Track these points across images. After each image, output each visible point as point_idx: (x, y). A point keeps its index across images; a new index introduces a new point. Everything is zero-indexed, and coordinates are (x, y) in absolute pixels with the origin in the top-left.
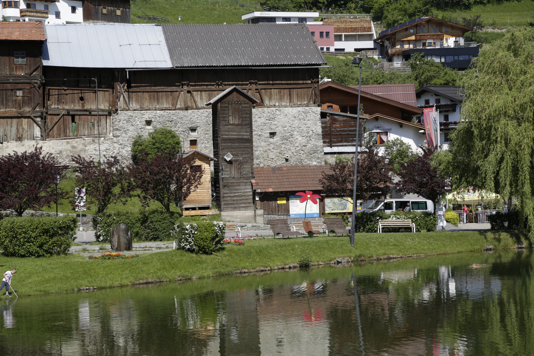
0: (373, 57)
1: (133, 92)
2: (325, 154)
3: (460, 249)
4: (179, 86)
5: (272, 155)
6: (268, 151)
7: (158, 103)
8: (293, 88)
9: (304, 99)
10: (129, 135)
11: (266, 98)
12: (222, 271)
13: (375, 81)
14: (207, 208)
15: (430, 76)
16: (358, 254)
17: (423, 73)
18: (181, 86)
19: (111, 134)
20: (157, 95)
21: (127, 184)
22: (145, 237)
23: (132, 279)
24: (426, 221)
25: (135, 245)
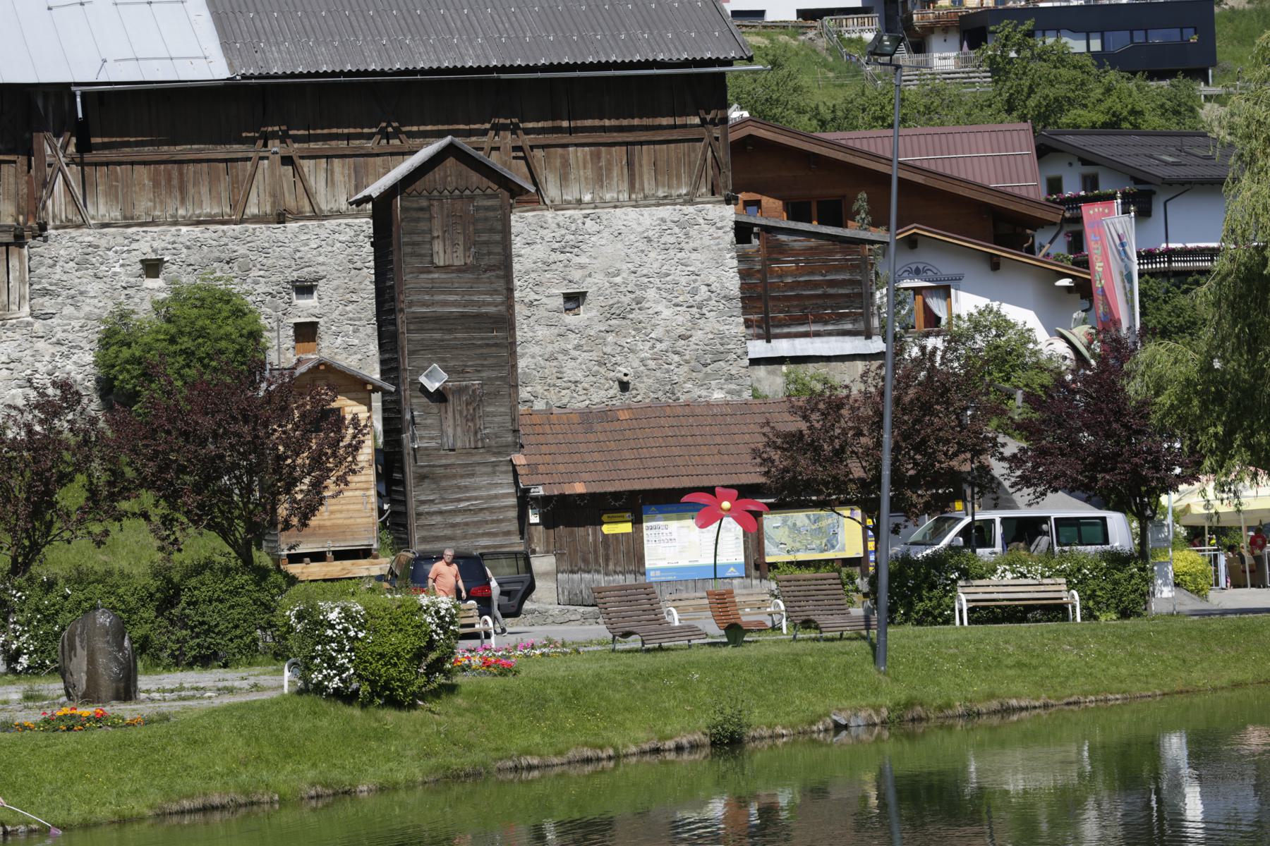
0: (860, 39)
1: (96, 164)
2: (755, 362)
3: (1234, 674)
4: (253, 141)
5: (572, 371)
6: (560, 357)
7: (183, 201)
8: (641, 143)
9: (679, 177)
10: (87, 309)
11: (551, 178)
12: (455, 763)
13: (876, 119)
14: (365, 553)
15: (1056, 99)
16: (903, 698)
17: (1031, 91)
18: (260, 142)
19: (26, 309)
20: (181, 174)
21: (105, 477)
22: (172, 655)
23: (156, 797)
24: (1116, 583)
25: (145, 682)
